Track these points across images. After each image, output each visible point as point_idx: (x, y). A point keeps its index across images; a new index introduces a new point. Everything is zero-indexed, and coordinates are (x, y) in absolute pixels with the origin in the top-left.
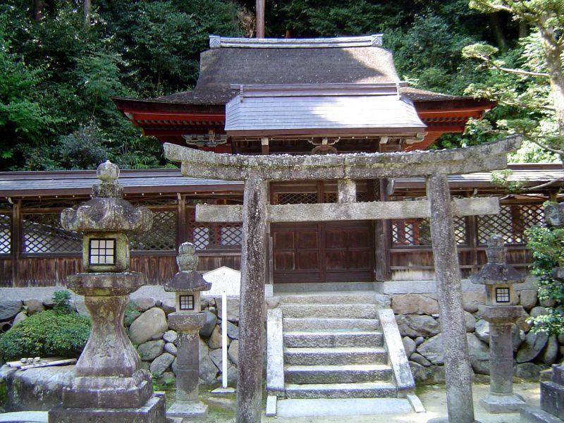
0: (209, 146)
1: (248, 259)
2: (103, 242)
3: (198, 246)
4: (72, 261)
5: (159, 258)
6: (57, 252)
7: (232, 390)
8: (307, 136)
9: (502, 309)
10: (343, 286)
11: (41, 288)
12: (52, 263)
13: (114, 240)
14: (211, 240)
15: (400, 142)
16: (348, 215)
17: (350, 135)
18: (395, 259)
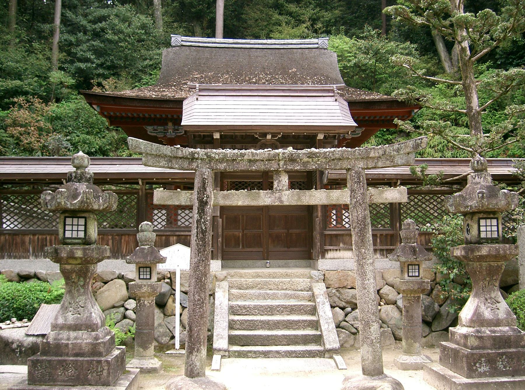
0: (169, 136)
1: (197, 236)
2: (75, 220)
3: (156, 226)
5: (121, 235)
6: (31, 228)
7: (183, 352)
8: (252, 131)
9: (412, 282)
10: (284, 263)
11: (16, 260)
12: (27, 239)
14: (168, 220)
15: (337, 137)
16: (281, 201)
18: (328, 241)
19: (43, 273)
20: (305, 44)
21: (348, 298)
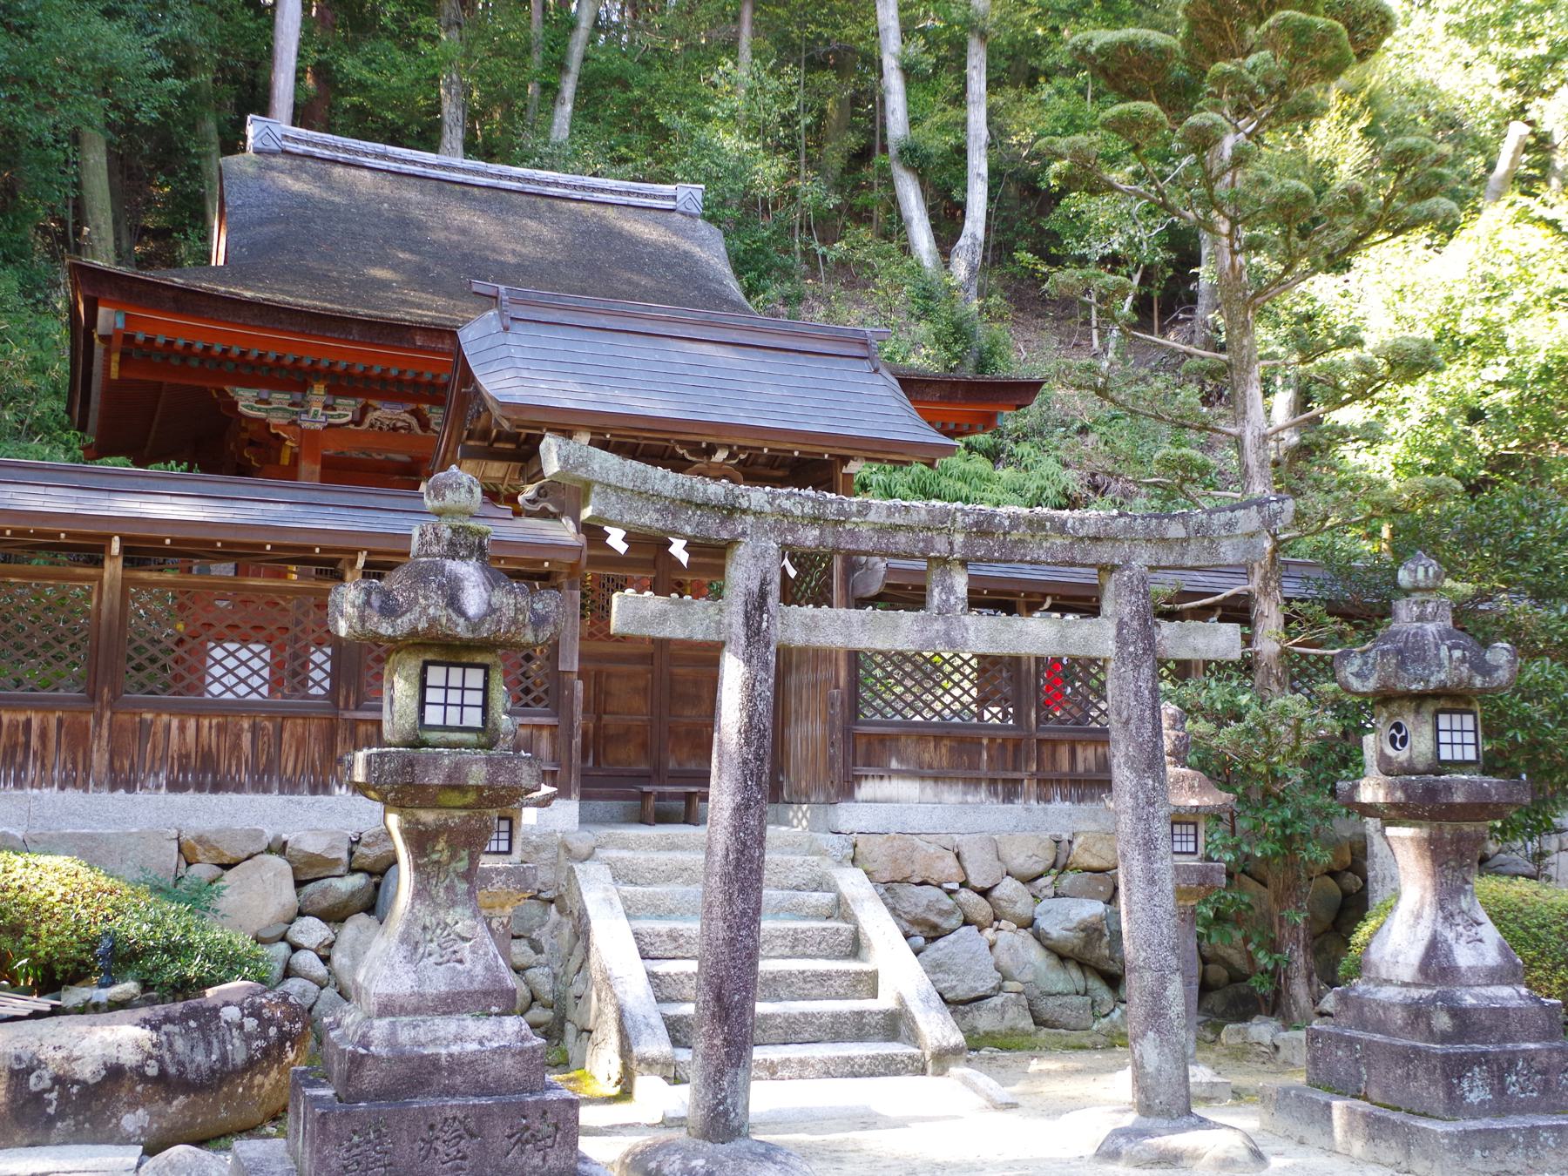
0: (306, 425)
2: (456, 673)
4: (21, 717)
13: (486, 668)
17: (788, 446)
19: (14, 837)
20: (638, 195)
21: (919, 910)
